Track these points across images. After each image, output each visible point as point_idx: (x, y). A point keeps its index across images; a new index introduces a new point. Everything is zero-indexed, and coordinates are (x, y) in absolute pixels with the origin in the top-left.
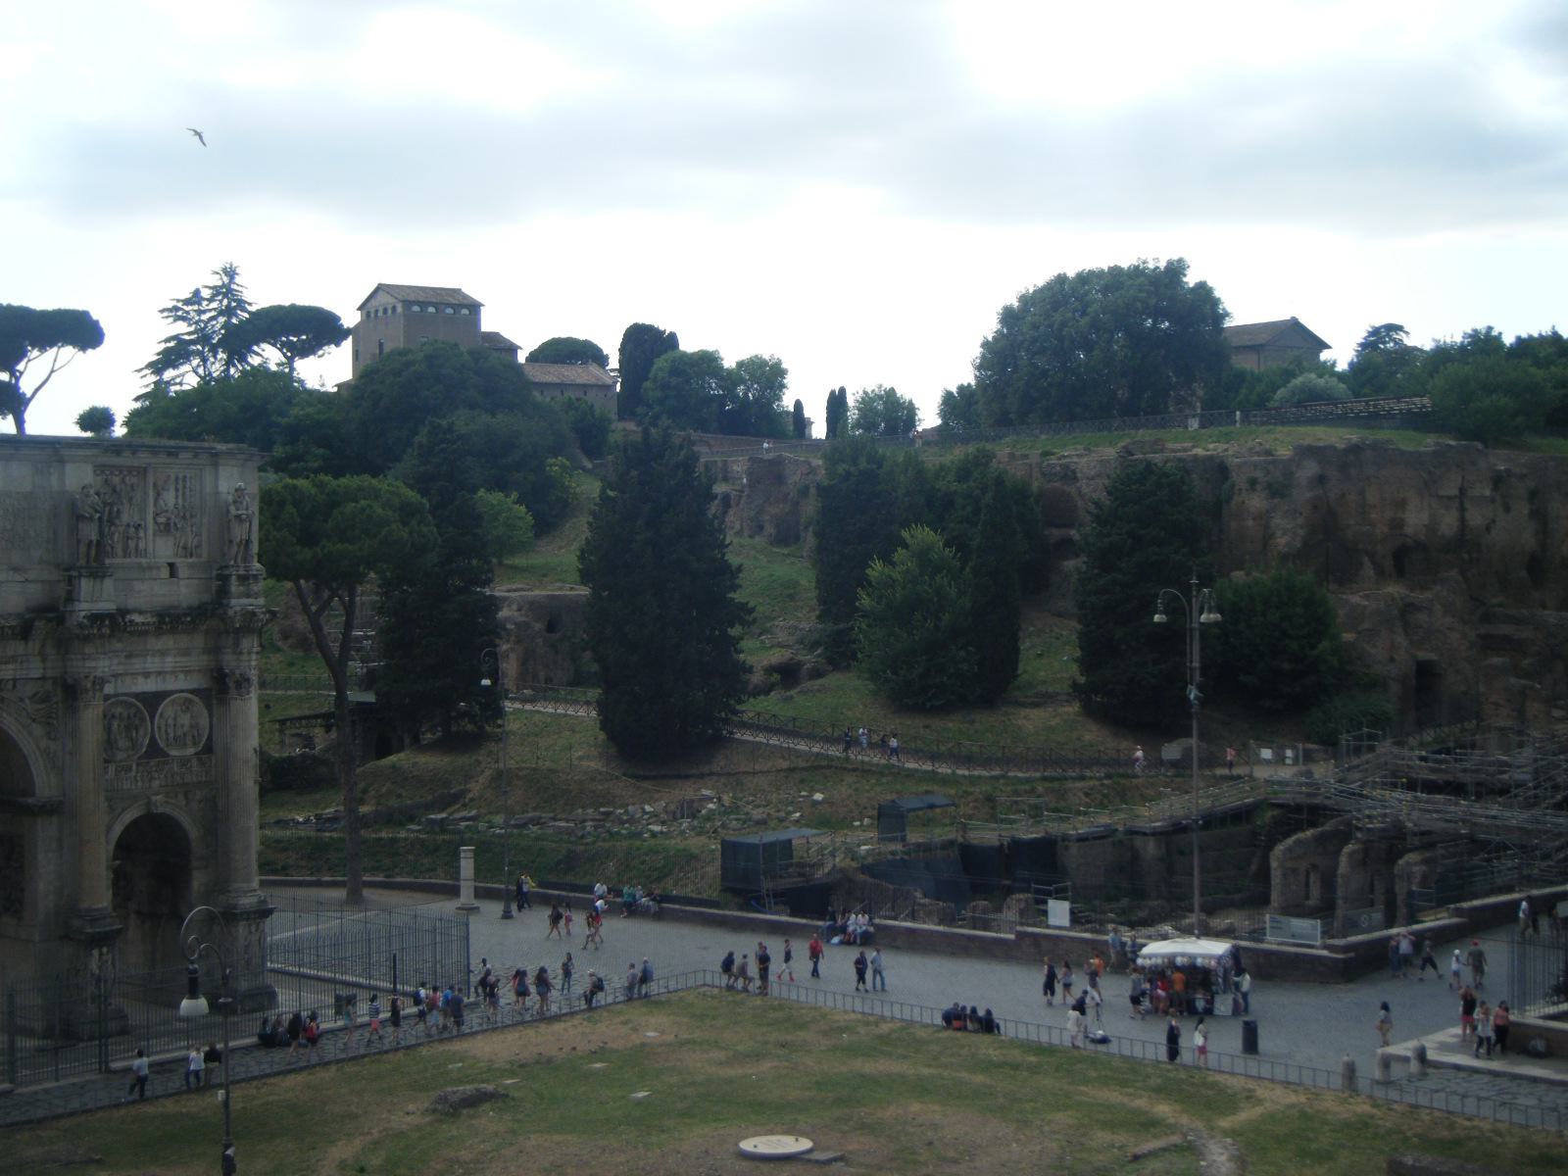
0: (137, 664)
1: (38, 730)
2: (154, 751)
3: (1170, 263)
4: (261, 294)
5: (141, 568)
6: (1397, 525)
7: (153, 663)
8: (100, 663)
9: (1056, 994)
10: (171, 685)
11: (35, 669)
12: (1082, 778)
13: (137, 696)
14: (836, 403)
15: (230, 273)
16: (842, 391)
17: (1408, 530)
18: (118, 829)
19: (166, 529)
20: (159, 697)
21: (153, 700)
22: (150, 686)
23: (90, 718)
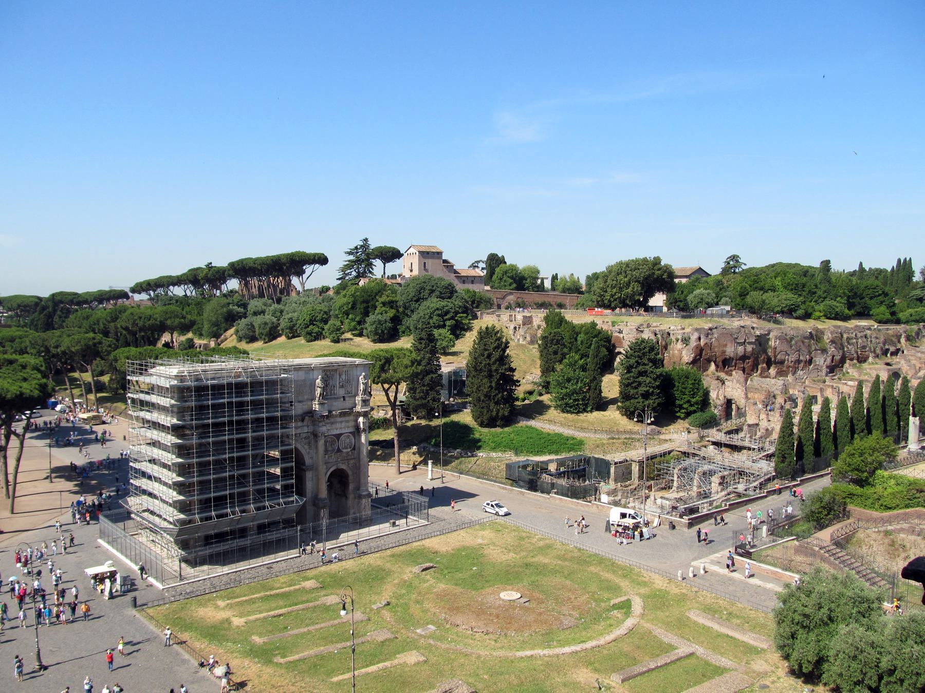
0: (334, 426)
1: (306, 447)
2: (339, 450)
3: (654, 258)
4: (373, 244)
5: (335, 398)
6: (724, 352)
7: (338, 425)
8: (323, 429)
9: (683, 320)
10: (343, 431)
11: (306, 430)
12: (619, 439)
13: (334, 435)
14: (555, 278)
15: (366, 240)
16: (557, 274)
17: (727, 353)
18: (329, 473)
19: (342, 387)
20: (341, 434)
21: (338, 436)
22: (338, 432)
23: (321, 443)
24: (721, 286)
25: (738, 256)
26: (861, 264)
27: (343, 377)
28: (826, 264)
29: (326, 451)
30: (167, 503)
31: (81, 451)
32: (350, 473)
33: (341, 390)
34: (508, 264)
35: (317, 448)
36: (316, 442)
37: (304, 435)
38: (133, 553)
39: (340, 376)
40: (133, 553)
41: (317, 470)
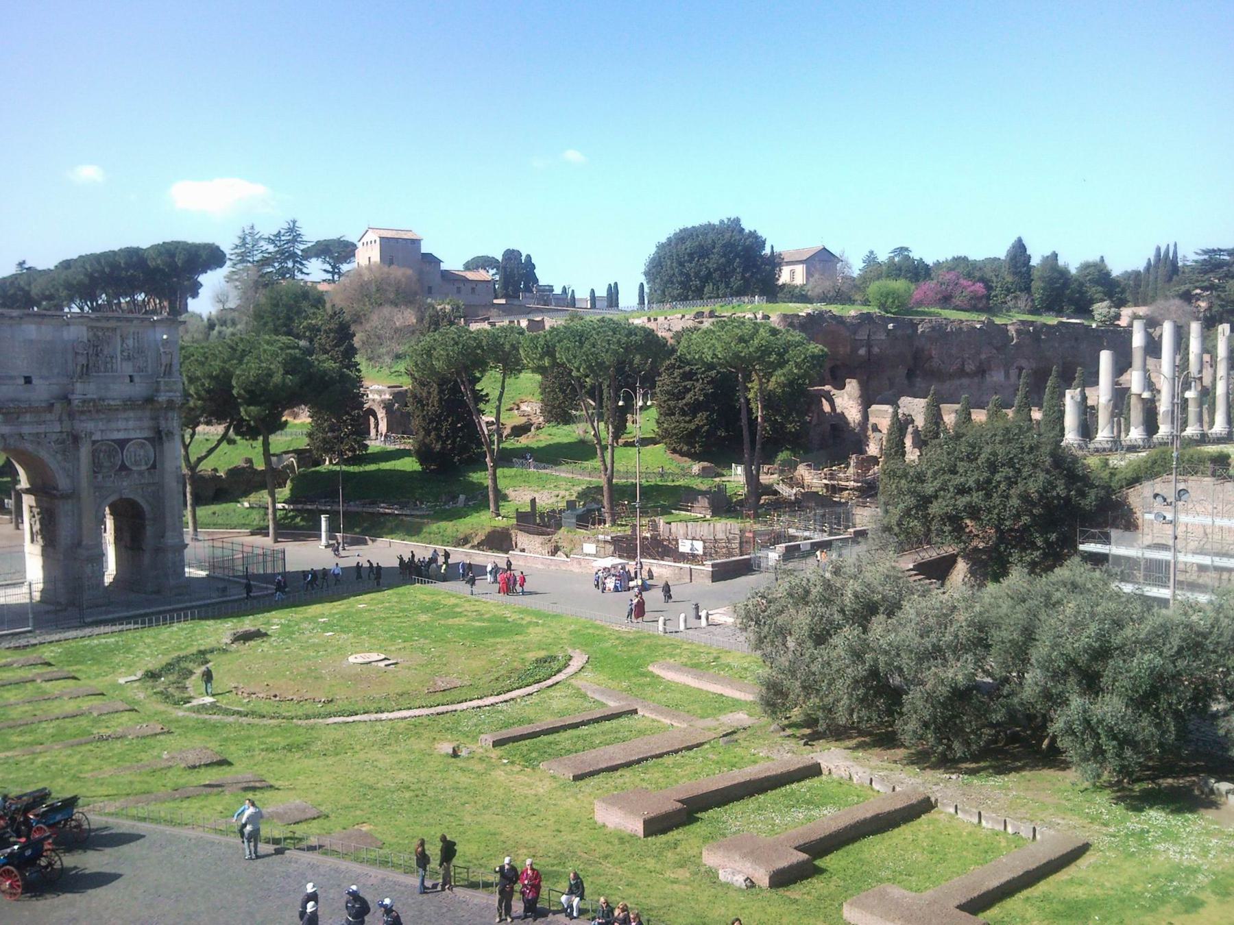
0: (113, 425)
1: (59, 457)
2: (123, 467)
7: (121, 424)
10: (132, 435)
13: (113, 441)
19: (129, 358)
20: (128, 440)
21: (122, 443)
23: (85, 452)
25: (907, 249)
26: (593, 291)
27: (130, 342)
28: (293, 229)
30: (272, 854)
33: (124, 364)
35: (78, 459)
36: (78, 449)
37: (54, 437)
39: (123, 341)
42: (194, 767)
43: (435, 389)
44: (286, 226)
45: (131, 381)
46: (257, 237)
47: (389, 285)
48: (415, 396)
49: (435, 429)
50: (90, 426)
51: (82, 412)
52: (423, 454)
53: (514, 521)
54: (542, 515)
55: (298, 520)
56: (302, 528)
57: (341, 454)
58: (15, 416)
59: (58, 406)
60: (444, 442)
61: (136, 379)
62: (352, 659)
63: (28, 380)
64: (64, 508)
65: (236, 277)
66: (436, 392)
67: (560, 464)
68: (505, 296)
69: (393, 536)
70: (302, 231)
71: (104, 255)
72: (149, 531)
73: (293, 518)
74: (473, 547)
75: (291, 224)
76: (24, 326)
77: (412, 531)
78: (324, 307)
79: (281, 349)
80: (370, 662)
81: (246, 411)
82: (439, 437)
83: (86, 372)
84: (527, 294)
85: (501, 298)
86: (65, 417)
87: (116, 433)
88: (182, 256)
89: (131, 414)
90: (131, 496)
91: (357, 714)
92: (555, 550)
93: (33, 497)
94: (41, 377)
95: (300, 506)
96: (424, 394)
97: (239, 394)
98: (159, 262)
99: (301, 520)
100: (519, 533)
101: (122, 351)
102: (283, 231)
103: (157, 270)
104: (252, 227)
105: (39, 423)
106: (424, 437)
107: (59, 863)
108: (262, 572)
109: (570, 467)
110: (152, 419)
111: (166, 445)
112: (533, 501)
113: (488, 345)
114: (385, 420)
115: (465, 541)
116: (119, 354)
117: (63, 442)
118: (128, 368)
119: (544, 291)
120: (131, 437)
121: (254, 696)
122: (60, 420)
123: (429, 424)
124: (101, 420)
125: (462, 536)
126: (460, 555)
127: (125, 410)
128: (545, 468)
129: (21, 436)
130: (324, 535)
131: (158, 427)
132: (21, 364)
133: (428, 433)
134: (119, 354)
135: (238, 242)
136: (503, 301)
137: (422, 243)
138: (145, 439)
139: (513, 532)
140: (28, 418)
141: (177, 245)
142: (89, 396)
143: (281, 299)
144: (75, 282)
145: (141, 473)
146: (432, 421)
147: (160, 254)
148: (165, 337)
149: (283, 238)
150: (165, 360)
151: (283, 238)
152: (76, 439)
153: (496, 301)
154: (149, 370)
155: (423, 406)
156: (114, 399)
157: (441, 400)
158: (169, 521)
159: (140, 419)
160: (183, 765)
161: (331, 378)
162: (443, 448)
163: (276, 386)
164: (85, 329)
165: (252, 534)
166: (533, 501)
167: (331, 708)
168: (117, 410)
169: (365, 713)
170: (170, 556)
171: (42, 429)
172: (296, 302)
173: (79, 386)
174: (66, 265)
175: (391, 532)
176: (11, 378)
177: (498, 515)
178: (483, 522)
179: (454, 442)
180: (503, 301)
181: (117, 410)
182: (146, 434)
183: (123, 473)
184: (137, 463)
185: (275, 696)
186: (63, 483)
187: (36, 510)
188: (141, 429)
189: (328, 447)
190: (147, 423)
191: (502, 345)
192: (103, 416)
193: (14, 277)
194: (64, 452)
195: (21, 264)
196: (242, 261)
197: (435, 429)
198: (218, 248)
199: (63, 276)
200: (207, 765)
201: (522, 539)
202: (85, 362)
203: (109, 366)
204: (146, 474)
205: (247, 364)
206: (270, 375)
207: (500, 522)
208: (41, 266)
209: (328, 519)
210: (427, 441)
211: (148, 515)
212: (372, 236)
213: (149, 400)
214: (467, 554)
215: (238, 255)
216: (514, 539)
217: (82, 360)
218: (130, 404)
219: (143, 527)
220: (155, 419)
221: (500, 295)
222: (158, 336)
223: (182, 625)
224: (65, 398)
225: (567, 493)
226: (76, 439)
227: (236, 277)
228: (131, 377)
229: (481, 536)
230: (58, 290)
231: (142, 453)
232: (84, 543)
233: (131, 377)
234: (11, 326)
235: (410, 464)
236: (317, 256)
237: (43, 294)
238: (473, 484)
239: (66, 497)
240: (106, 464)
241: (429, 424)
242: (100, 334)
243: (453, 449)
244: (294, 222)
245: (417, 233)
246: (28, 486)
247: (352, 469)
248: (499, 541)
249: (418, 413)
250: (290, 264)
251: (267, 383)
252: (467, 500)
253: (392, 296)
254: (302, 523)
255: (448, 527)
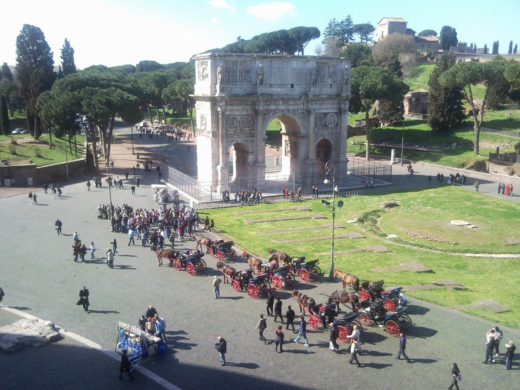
0: (323, 106)
1: (302, 120)
2: (325, 125)
7: (326, 106)
13: (322, 113)
18: (317, 142)
19: (330, 76)
20: (328, 113)
21: (326, 114)
23: (312, 118)
24: (214, 58)
27: (331, 69)
28: (348, 20)
29: (316, 124)
31: (99, 184)
32: (333, 143)
33: (329, 79)
34: (322, 29)
35: (309, 121)
37: (301, 111)
38: (194, 191)
40: (194, 191)
41: (309, 138)
42: (420, 272)
43: (443, 93)
44: (346, 18)
45: (331, 87)
46: (336, 23)
47: (402, 43)
48: (432, 95)
49: (441, 111)
50: (315, 106)
51: (313, 100)
52: (434, 123)
53: (488, 158)
54: (501, 156)
55: (376, 151)
56: (378, 154)
57: (391, 121)
58: (287, 101)
59: (303, 97)
60: (445, 118)
61: (333, 86)
62: (452, 222)
63: (292, 86)
64: (302, 143)
65: (326, 41)
66: (443, 93)
67: (501, 130)
68: (444, 48)
69: (425, 161)
70: (352, 20)
71: (272, 33)
72: (333, 153)
73: (374, 150)
74: (467, 169)
75: (348, 17)
76: (292, 62)
77: (434, 159)
78: (371, 54)
79: (380, 72)
80: (463, 225)
81: (365, 102)
82: (443, 115)
83: (315, 83)
84: (454, 47)
85: (441, 49)
86: (305, 103)
87: (323, 110)
88: (303, 33)
89: (329, 102)
90: (328, 138)
91: (479, 253)
92: (513, 173)
93: (287, 136)
94: (298, 85)
95: (377, 145)
96: (437, 95)
97: (362, 94)
98: (294, 36)
99: (377, 151)
100: (491, 164)
101: (328, 73)
102: (344, 21)
103: (293, 39)
104: (334, 19)
105: (296, 105)
106: (435, 115)
107: (269, 286)
108: (383, 174)
109: (506, 132)
110: (338, 104)
111: (343, 116)
112: (498, 148)
113: (485, 71)
114: (408, 106)
115: (463, 166)
116: (327, 75)
117: (303, 113)
118: (329, 81)
119: (462, 45)
120: (329, 112)
121: (416, 237)
122: (303, 104)
123: (438, 109)
124: (319, 104)
125: (461, 163)
126: (462, 172)
127: (328, 100)
128: (495, 132)
129: (288, 110)
130: (392, 158)
131: (340, 108)
132: (290, 79)
133: (437, 112)
134: (327, 75)
135: (328, 26)
136: (442, 51)
137: (408, 24)
138: (334, 113)
139: (487, 163)
140: (291, 102)
141: (301, 28)
142: (315, 93)
143: (352, 51)
144: (261, 45)
145: (332, 128)
146: (440, 107)
147: (294, 32)
148: (346, 67)
149: (344, 24)
150: (346, 77)
151: (344, 24)
152: (309, 112)
153: (439, 51)
154: (338, 82)
155: (436, 100)
156: (324, 95)
157: (445, 97)
158: (342, 149)
159: (333, 104)
160: (414, 271)
161: (399, 86)
162: (444, 120)
163: (379, 90)
164: (314, 63)
165: (356, 156)
166: (498, 148)
167: (457, 248)
168: (325, 99)
169: (483, 253)
170: (342, 165)
171: (296, 107)
172: (359, 52)
173: (312, 89)
174: (256, 38)
175: (423, 159)
176: (287, 85)
177: (478, 154)
178: (470, 157)
179: (449, 118)
180: (442, 51)
181: (325, 99)
182: (335, 111)
183: (325, 128)
184: (331, 124)
185: (428, 238)
186: (303, 131)
187: (288, 142)
188: (333, 108)
189: (386, 118)
190: (336, 106)
191: (493, 70)
192: (319, 102)
193: (236, 44)
194: (304, 118)
195: (239, 38)
196: (329, 34)
197: (441, 111)
198: (317, 29)
199: (257, 43)
200: (425, 272)
201: (491, 166)
202: (315, 79)
203: (323, 80)
204: (334, 128)
205: (365, 79)
206: (376, 85)
207: (480, 158)
208: (246, 39)
209: (395, 151)
210: (436, 117)
211: (333, 147)
212: (385, 21)
213: (338, 95)
214: (466, 172)
215: (328, 32)
216: (487, 166)
217: (314, 77)
218: (330, 97)
219: (331, 151)
220: (339, 104)
221: (440, 48)
222: (343, 67)
223: (355, 196)
224: (306, 94)
225: (509, 145)
226: (309, 112)
227: (326, 41)
228: (331, 85)
229: (472, 164)
230: (254, 49)
231: (333, 119)
232: (310, 158)
233: (331, 85)
234: (287, 62)
235: (425, 127)
236: (356, 32)
237: (249, 51)
238: (457, 138)
239: (303, 137)
240: (319, 123)
241: (438, 109)
242: (320, 65)
243: (449, 121)
244: (349, 16)
245: (405, 20)
246: (285, 132)
247: (397, 128)
248: (480, 166)
249: (433, 103)
250: (346, 36)
251: (375, 88)
252: (457, 146)
253: (403, 49)
254: (378, 152)
255: (456, 159)
